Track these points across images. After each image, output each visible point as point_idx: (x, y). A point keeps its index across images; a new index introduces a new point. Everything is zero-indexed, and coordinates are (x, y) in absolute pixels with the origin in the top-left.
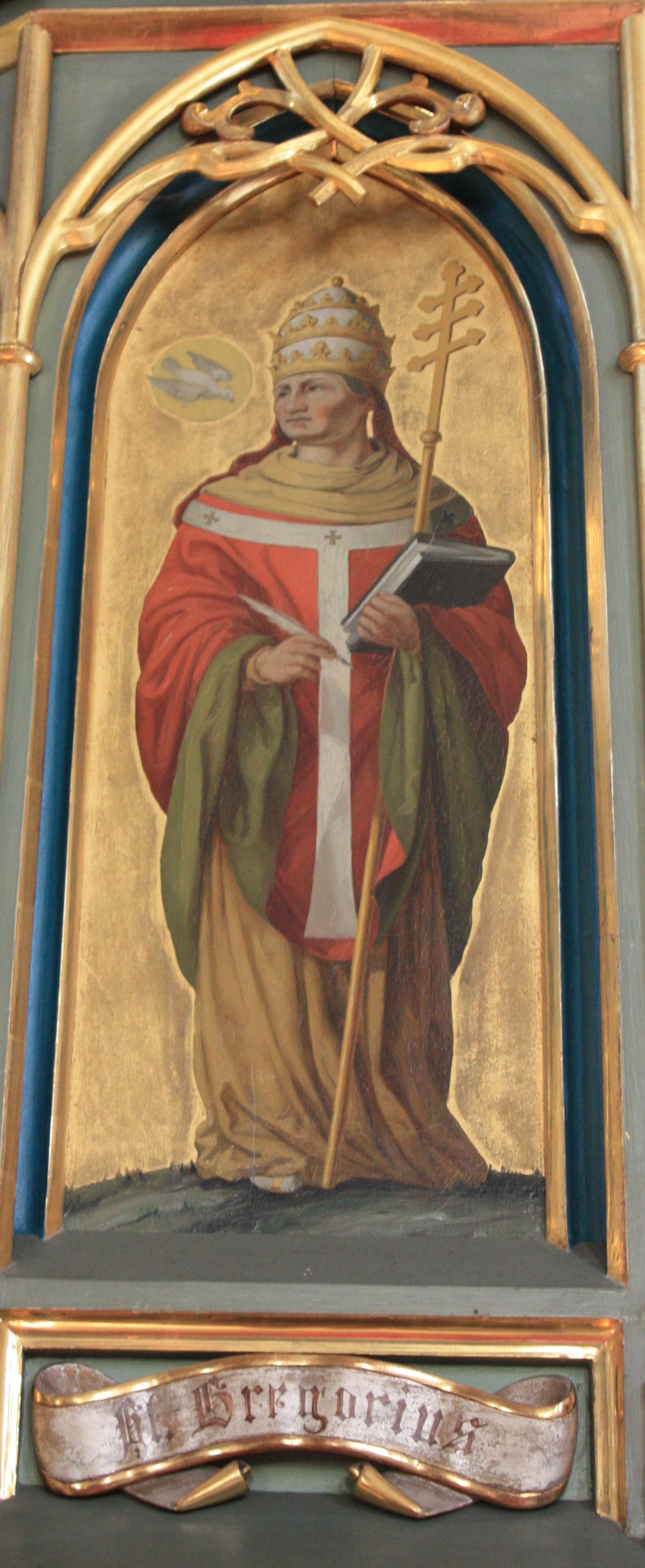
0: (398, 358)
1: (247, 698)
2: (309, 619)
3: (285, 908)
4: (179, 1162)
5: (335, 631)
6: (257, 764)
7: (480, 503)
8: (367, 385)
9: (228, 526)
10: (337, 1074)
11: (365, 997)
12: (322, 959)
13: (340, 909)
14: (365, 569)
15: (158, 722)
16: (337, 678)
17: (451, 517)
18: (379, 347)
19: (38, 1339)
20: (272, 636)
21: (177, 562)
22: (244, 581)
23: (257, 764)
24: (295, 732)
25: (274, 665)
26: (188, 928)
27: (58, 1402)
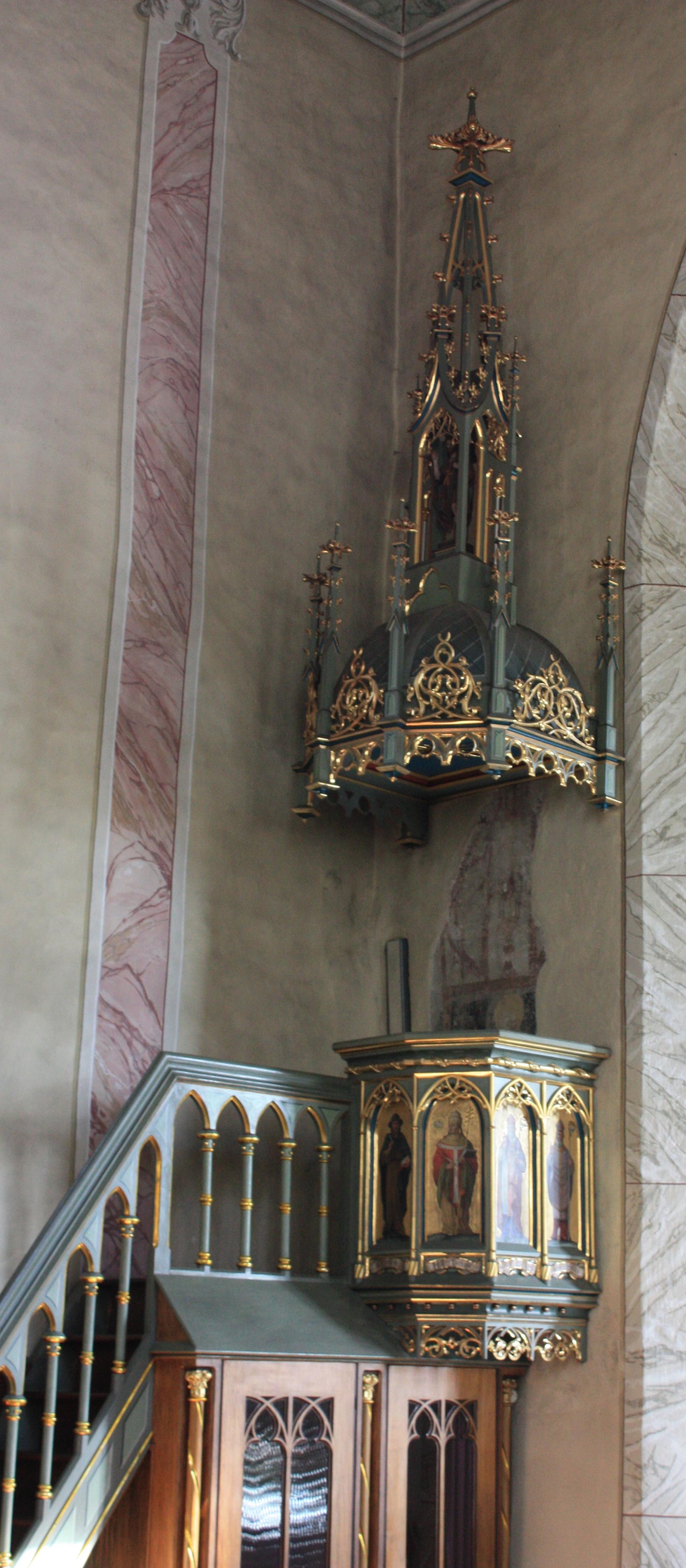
0: (463, 1121)
1: (446, 1171)
2: (452, 1159)
3: (450, 1200)
4: (646, 1112)
5: (456, 1162)
6: (447, 1180)
7: (473, 1143)
8: (459, 1125)
9: (443, 1146)
10: (457, 1221)
11: (460, 1211)
12: (454, 1206)
13: (457, 1200)
14: (460, 1152)
15: (436, 1173)
16: (456, 1168)
17: (470, 1145)
18: (460, 1119)
19: (428, 1208)
20: (448, 1162)
21: (437, 1152)
22: (446, 1155)
23: (447, 1180)
24: (307, 1544)
25: (449, 1166)
26: (440, 1201)
27: (365, 711)
